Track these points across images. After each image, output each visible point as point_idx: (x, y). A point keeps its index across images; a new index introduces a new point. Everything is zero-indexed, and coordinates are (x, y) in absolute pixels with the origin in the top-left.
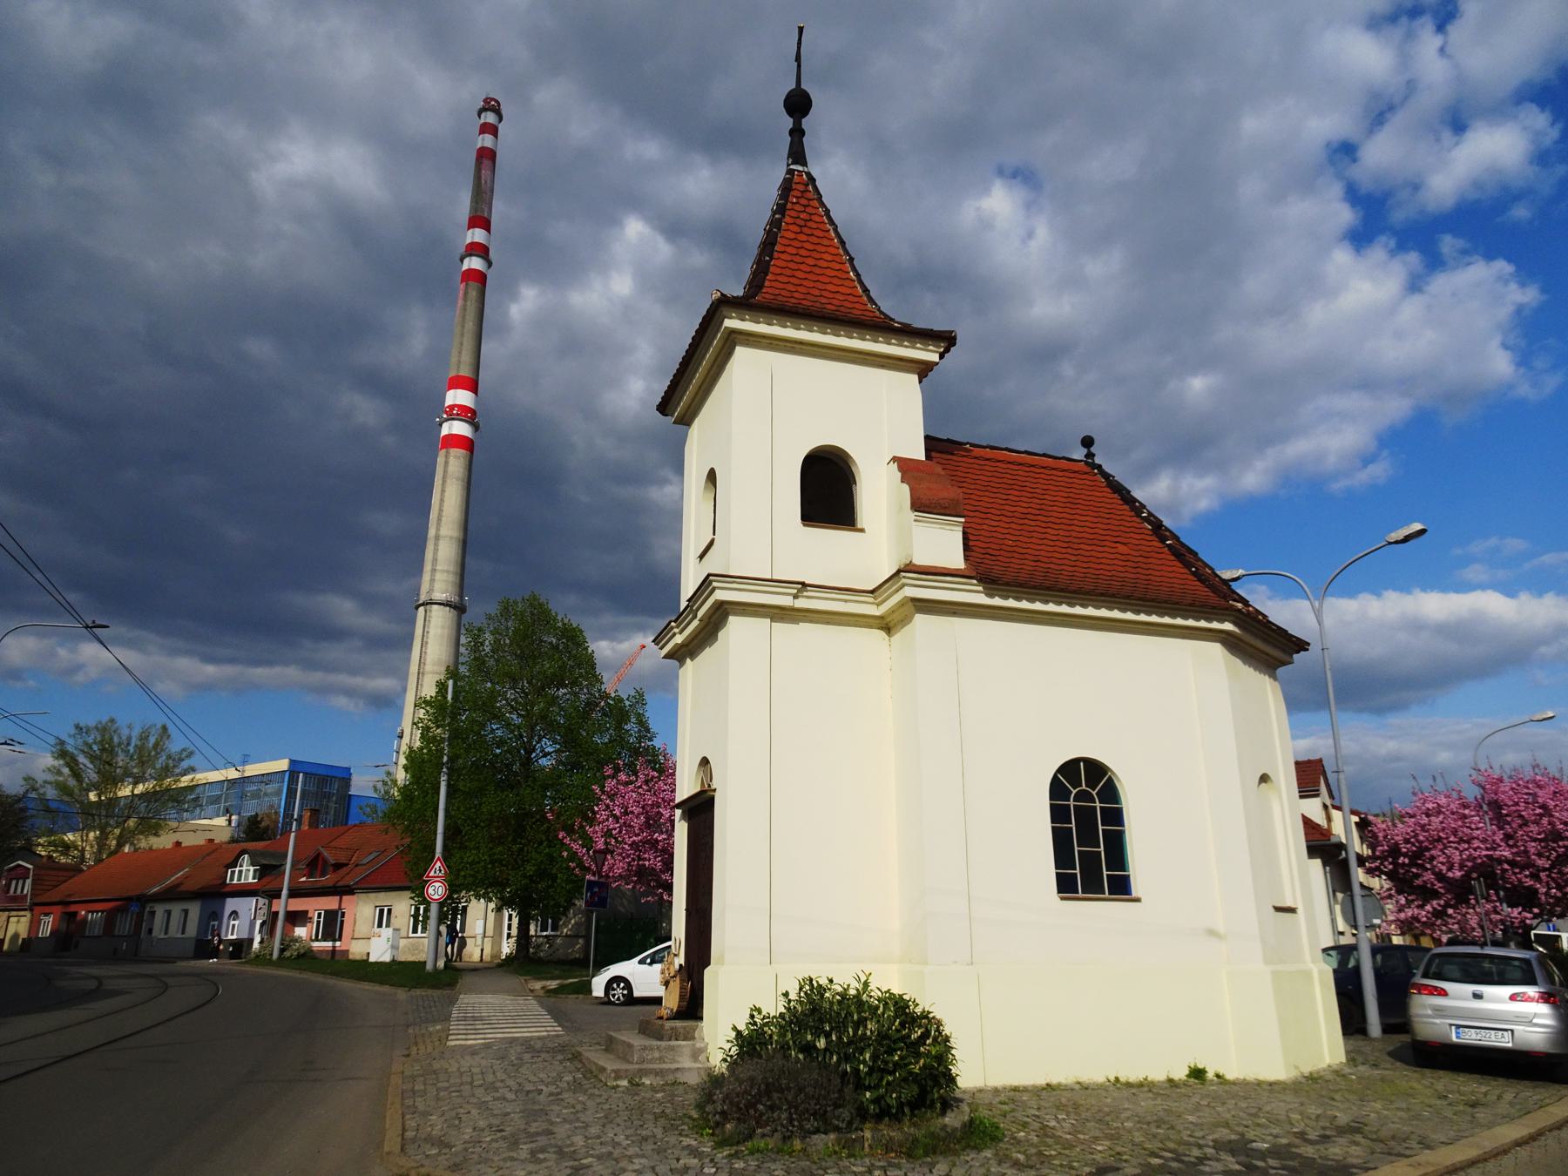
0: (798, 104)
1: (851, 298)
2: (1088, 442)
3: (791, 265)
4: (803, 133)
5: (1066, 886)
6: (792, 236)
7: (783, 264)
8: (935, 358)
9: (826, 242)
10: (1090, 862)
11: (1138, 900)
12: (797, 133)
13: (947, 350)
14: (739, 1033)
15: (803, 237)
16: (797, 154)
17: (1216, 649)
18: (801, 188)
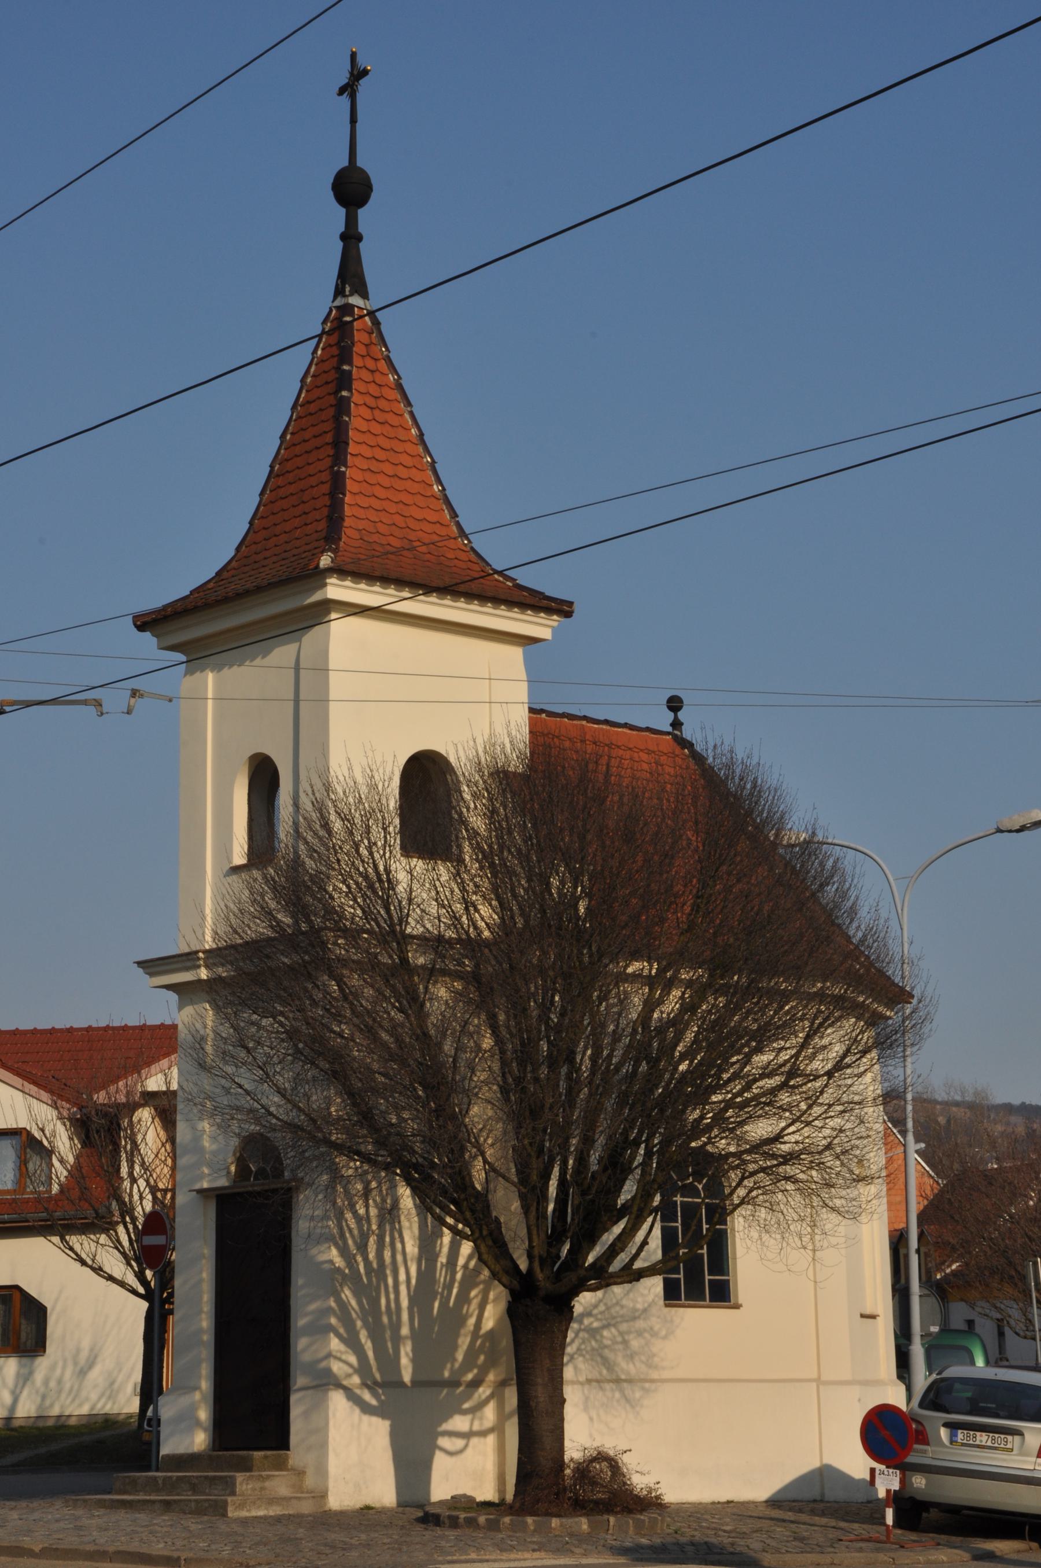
0: (352, 189)
2: (675, 704)
5: (721, 1294)
11: (737, 1306)
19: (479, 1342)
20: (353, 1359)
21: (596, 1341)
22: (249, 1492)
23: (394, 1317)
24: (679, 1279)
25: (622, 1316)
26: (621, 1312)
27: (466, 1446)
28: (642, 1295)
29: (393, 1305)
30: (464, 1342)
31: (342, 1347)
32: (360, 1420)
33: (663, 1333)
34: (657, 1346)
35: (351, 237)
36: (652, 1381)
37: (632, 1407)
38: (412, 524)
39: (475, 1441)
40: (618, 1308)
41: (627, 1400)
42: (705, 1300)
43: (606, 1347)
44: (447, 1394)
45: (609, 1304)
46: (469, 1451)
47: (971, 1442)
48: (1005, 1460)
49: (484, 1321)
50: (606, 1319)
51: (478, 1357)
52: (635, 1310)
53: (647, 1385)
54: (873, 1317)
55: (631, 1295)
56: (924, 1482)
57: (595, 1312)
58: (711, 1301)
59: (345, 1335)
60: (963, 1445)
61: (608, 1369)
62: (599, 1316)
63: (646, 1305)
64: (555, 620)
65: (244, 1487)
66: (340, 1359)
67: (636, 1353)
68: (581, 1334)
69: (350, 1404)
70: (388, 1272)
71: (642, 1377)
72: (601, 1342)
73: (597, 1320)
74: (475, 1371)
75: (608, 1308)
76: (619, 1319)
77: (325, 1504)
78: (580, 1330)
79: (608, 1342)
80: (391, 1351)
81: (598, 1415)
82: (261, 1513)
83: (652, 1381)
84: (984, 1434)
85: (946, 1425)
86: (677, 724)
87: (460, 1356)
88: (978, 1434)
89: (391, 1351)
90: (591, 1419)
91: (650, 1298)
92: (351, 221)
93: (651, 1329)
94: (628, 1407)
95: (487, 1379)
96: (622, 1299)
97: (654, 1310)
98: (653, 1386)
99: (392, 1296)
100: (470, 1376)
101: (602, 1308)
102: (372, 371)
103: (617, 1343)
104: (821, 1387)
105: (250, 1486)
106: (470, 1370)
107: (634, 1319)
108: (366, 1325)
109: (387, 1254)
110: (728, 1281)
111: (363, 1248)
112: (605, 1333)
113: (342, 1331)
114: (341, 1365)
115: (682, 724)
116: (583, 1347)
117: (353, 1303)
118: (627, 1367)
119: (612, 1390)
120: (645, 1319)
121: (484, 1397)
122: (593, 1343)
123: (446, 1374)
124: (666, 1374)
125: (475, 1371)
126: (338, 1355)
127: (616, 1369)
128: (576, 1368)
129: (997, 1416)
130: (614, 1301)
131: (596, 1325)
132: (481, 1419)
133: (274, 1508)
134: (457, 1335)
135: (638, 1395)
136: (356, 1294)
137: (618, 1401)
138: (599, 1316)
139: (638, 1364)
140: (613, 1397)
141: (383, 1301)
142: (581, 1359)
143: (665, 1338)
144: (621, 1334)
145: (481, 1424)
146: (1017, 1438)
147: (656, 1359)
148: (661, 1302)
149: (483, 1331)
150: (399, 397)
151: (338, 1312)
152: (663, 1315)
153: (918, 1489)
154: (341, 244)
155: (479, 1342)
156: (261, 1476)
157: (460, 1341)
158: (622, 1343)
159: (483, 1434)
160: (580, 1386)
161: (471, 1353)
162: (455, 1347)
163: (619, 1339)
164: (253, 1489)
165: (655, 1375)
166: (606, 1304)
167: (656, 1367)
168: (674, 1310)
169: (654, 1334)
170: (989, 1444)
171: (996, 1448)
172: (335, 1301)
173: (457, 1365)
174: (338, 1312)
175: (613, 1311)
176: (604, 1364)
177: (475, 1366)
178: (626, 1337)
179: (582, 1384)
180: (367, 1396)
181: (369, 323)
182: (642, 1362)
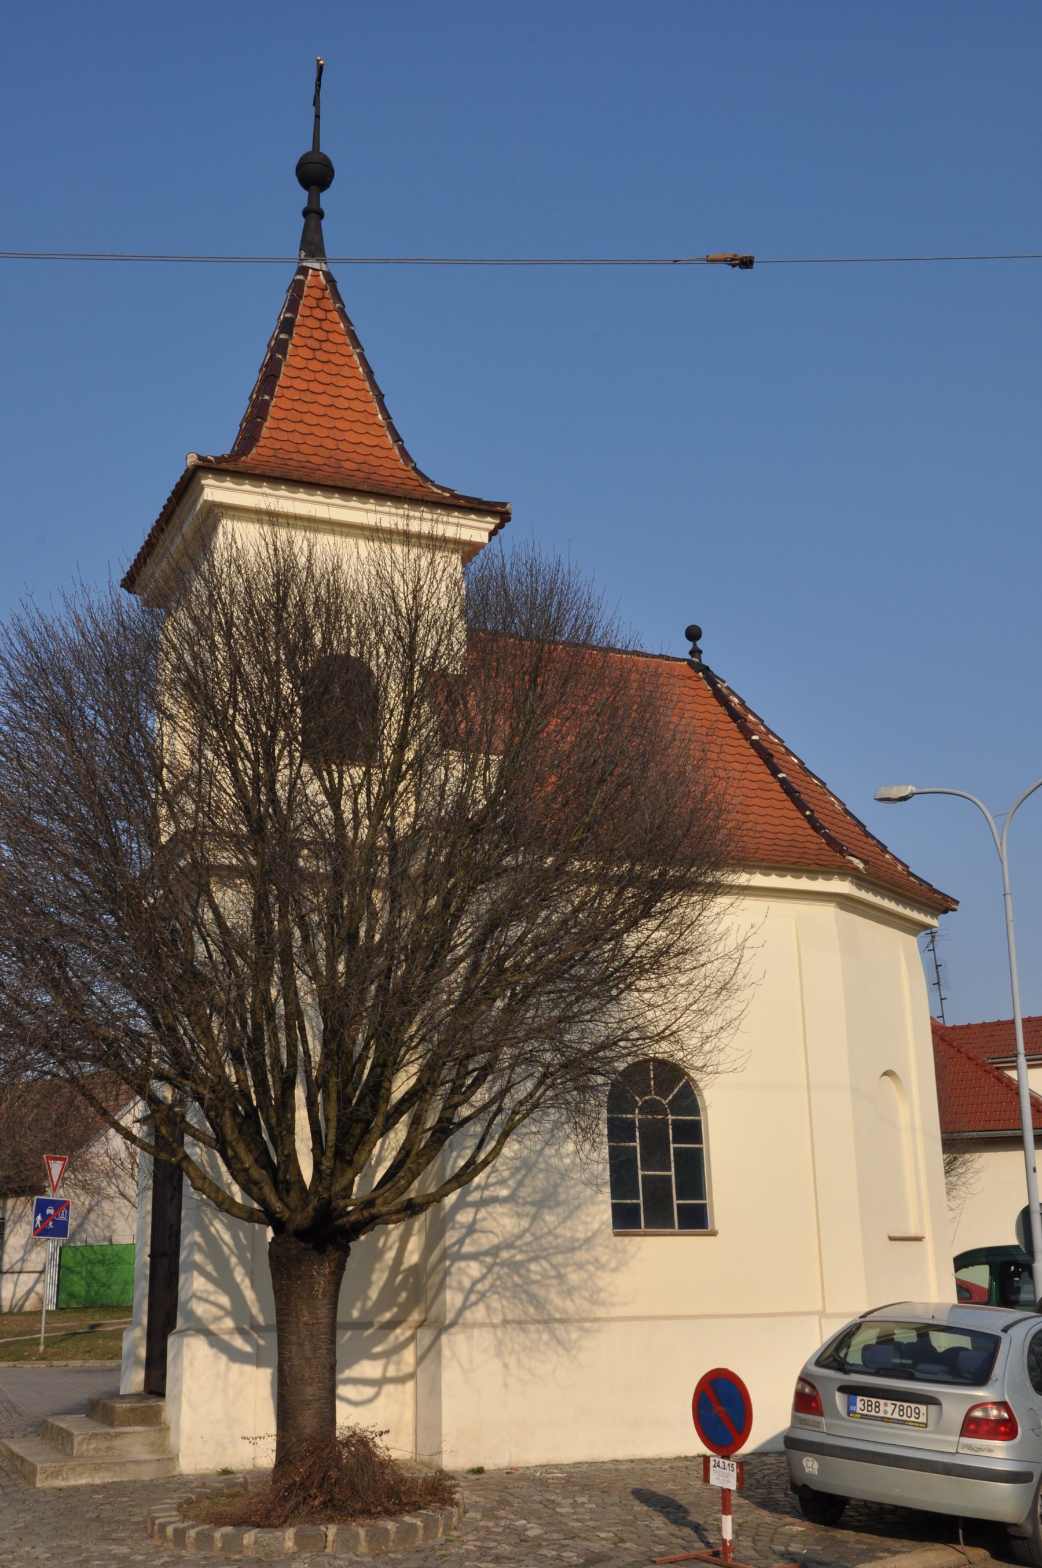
0: (315, 174)
1: (377, 452)
2: (693, 634)
3: (298, 406)
4: (321, 215)
5: (696, 1220)
6: (302, 364)
7: (288, 405)
8: (482, 537)
9: (346, 371)
10: (657, 1192)
11: (714, 1234)
12: (313, 214)
13: (500, 526)
14: (706, 1530)
15: (315, 365)
16: (313, 244)
17: (829, 911)
18: (318, 293)
19: (400, 1278)
20: (224, 1300)
21: (520, 1276)
22: (91, 1453)
25: (556, 1247)
26: (555, 1243)
27: (376, 1395)
28: (584, 1223)
30: (379, 1278)
31: (210, 1287)
32: (228, 1369)
33: (613, 1264)
34: (604, 1279)
36: (596, 1320)
37: (567, 1350)
38: (343, 446)
39: (388, 1389)
40: (550, 1238)
41: (560, 1342)
42: (673, 1227)
43: (534, 1282)
44: (351, 1338)
45: (539, 1233)
46: (381, 1400)
47: (873, 1413)
48: (916, 1439)
49: (407, 1254)
50: (533, 1251)
51: (399, 1294)
52: (574, 1240)
53: (587, 1325)
54: (919, 1239)
55: (569, 1223)
56: (816, 1466)
57: (519, 1243)
58: (680, 1227)
59: (214, 1274)
60: (863, 1416)
61: (536, 1307)
62: (525, 1248)
63: (589, 1234)
64: (490, 523)
65: (85, 1447)
66: (206, 1301)
68: (496, 1269)
69: (214, 1351)
71: (583, 1315)
72: (528, 1277)
73: (521, 1252)
74: (395, 1310)
75: (537, 1239)
76: (551, 1251)
77: (174, 1468)
78: (494, 1264)
79: (534, 1277)
81: (519, 1360)
82: (82, 1481)
83: (596, 1320)
84: (889, 1402)
85: (843, 1389)
86: (696, 652)
87: (374, 1293)
88: (882, 1402)
90: (506, 1366)
91: (596, 1225)
92: (314, 200)
93: (597, 1260)
94: (561, 1351)
95: (410, 1319)
96: (555, 1228)
97: (600, 1240)
98: (596, 1326)
100: (387, 1316)
101: (528, 1238)
102: (320, 320)
103: (549, 1277)
104: (823, 1320)
105: (92, 1447)
106: (389, 1309)
107: (573, 1250)
108: (242, 1262)
110: (705, 1205)
112: (533, 1267)
113: (210, 1268)
114: (208, 1306)
115: (701, 652)
116: (498, 1283)
117: (227, 1237)
118: (558, 1303)
119: (538, 1331)
120: (588, 1250)
121: (402, 1338)
122: (516, 1279)
123: (355, 1314)
124: (616, 1312)
125: (395, 1310)
126: (204, 1295)
127: (547, 1307)
128: (488, 1308)
129: (911, 1377)
130: (546, 1230)
131: (519, 1257)
132: (398, 1363)
133: (101, 1474)
134: (371, 1270)
135: (574, 1336)
137: (546, 1344)
138: (525, 1248)
139: (578, 1301)
140: (540, 1338)
142: (496, 1297)
143: (615, 1270)
144: (554, 1267)
145: (398, 1370)
146: (933, 1408)
147: (603, 1295)
148: (610, 1230)
149: (405, 1265)
150: (348, 341)
151: (205, 1247)
153: (811, 1475)
154: (304, 220)
155: (400, 1278)
156: (108, 1434)
157: (375, 1277)
158: (555, 1277)
159: (401, 1380)
160: (491, 1329)
161: (389, 1293)
162: (369, 1284)
163: (553, 1273)
164: (97, 1450)
165: (601, 1313)
166: (533, 1234)
167: (603, 1304)
168: (627, 1239)
169: (602, 1267)
170: (896, 1416)
171: (904, 1422)
172: (202, 1236)
173: (369, 1304)
174: (205, 1247)
176: (531, 1303)
177: (395, 1304)
178: (562, 1271)
179: (494, 1326)
180: (238, 1342)
181: (324, 282)
182: (585, 1298)
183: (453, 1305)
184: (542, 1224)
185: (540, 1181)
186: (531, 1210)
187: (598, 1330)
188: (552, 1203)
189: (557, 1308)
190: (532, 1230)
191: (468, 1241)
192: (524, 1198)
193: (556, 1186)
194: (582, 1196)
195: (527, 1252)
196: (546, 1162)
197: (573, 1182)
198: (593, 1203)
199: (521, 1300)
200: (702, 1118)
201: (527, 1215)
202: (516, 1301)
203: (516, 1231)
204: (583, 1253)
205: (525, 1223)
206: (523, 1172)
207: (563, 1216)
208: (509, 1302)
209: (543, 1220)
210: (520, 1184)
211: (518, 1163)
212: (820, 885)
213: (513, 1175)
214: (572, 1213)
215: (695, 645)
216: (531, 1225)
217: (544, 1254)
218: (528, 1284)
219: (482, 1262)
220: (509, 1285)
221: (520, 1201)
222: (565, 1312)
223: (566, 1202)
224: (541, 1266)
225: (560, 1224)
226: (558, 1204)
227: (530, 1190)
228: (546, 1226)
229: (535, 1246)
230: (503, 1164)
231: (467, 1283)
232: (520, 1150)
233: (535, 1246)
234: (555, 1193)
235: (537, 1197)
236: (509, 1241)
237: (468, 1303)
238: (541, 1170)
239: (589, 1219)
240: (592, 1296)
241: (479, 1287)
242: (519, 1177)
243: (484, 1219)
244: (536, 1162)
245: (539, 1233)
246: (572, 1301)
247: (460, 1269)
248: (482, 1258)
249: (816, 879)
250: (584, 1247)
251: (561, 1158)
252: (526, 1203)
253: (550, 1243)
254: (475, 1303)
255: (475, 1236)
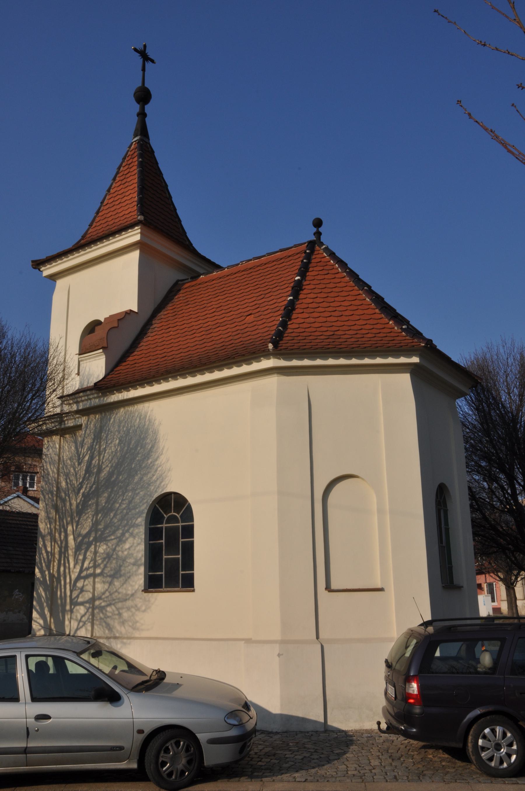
0: (143, 96)
2: (318, 223)
17: (274, 380)
20: (41, 622)
21: (103, 613)
23: (63, 601)
24: (162, 575)
25: (119, 599)
28: (132, 586)
29: (63, 595)
31: (38, 616)
33: (143, 608)
34: (139, 616)
35: (142, 115)
40: (116, 594)
42: (179, 587)
43: (108, 617)
50: (109, 601)
52: (127, 595)
53: (125, 641)
54: (381, 590)
55: (125, 586)
57: (103, 597)
59: (39, 610)
63: (134, 591)
67: (125, 620)
70: (62, 578)
72: (106, 614)
73: (104, 601)
75: (111, 594)
76: (117, 601)
79: (109, 614)
80: (61, 618)
89: (61, 618)
92: (143, 109)
93: (136, 606)
96: (119, 589)
98: (129, 641)
99: (63, 590)
103: (115, 615)
107: (126, 600)
109: (62, 569)
111: (48, 569)
112: (109, 609)
117: (43, 594)
120: (132, 600)
122: (101, 615)
124: (144, 634)
126: (36, 619)
127: (114, 630)
130: (115, 590)
131: (103, 604)
136: (45, 590)
138: (105, 599)
141: (59, 593)
143: (144, 611)
144: (118, 609)
147: (138, 624)
152: (142, 598)
158: (118, 615)
163: (116, 612)
165: (137, 634)
166: (109, 592)
168: (150, 594)
169: (138, 609)
175: (114, 596)
176: (106, 627)
178: (121, 611)
182: (130, 626)
183: (73, 628)
184: (113, 587)
185: (113, 564)
186: (109, 579)
187: (129, 644)
188: (118, 576)
189: (117, 631)
190: (109, 590)
191: (80, 596)
192: (106, 573)
193: (120, 566)
194: (131, 572)
195: (106, 601)
196: (117, 555)
197: (127, 564)
198: (136, 575)
199: (103, 626)
200: (148, 526)
201: (107, 582)
202: (101, 627)
203: (103, 591)
204: (130, 602)
205: (106, 586)
206: (107, 560)
207: (122, 582)
208: (98, 627)
209: (114, 585)
210: (105, 566)
211: (105, 556)
212: (255, 366)
213: (103, 562)
214: (126, 580)
215: (318, 230)
216: (109, 587)
217: (114, 602)
218: (106, 618)
219: (85, 606)
220: (98, 618)
221: (105, 575)
222: (121, 633)
223: (124, 574)
224: (112, 609)
225: (121, 586)
226: (121, 576)
227: (109, 569)
228: (115, 587)
229: (110, 598)
230: (99, 557)
231: (79, 617)
232: (106, 549)
233: (110, 598)
234: (120, 570)
235: (112, 573)
236: (99, 596)
237: (79, 627)
238: (114, 559)
239: (134, 584)
240: (133, 625)
241: (84, 619)
242: (105, 563)
243: (87, 585)
244: (113, 555)
245: (112, 592)
246: (124, 627)
247: (77, 610)
248: (85, 604)
249: (251, 363)
250: (131, 599)
251: (123, 552)
252: (107, 576)
253: (116, 596)
254: (81, 627)
255: (83, 593)
